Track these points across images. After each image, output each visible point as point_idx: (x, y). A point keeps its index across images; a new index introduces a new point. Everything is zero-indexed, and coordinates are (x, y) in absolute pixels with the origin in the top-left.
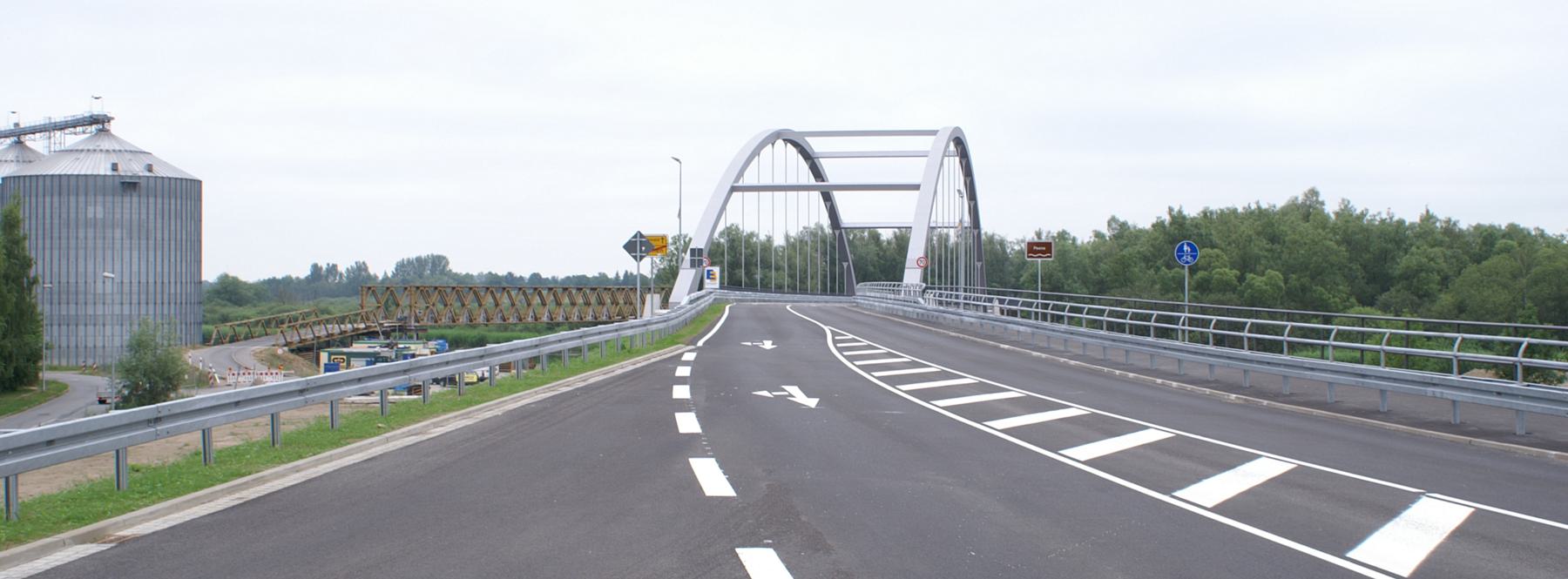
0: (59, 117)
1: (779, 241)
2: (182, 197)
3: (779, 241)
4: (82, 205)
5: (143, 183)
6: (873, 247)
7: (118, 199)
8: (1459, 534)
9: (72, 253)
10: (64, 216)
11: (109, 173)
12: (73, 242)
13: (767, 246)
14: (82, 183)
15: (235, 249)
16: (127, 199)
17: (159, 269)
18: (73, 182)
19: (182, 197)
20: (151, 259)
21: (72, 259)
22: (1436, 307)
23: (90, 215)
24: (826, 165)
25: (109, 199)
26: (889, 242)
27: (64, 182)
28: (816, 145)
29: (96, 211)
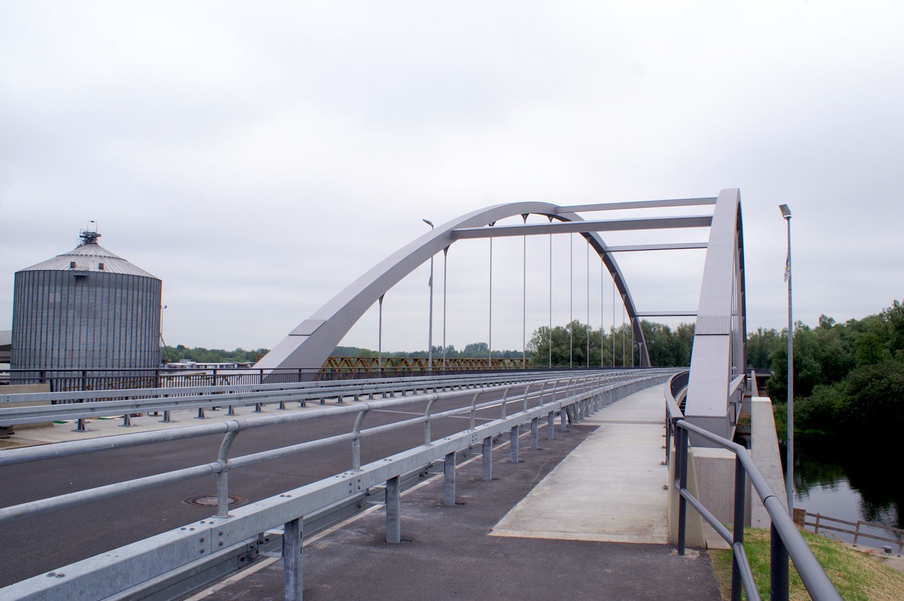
0: (792, 250)
1: (607, 332)
2: (147, 290)
3: (607, 332)
4: (46, 292)
5: (92, 276)
6: (665, 336)
7: (72, 288)
8: (495, 521)
9: (57, 328)
10: (35, 300)
11: (98, 270)
12: (39, 319)
13: (597, 336)
14: (59, 276)
15: (174, 332)
16: (79, 289)
17: (123, 342)
18: (59, 275)
19: (147, 290)
20: (117, 334)
21: (56, 332)
22: (582, 355)
23: (52, 300)
24: (619, 259)
25: (72, 288)
26: (675, 334)
27: (59, 276)
28: (608, 238)
29: (55, 297)
